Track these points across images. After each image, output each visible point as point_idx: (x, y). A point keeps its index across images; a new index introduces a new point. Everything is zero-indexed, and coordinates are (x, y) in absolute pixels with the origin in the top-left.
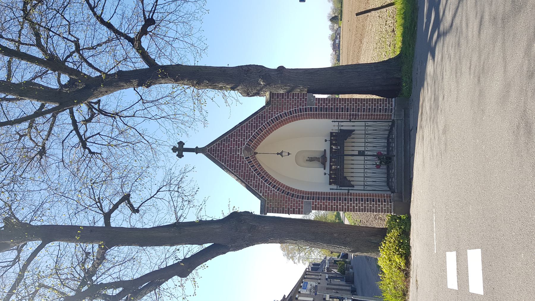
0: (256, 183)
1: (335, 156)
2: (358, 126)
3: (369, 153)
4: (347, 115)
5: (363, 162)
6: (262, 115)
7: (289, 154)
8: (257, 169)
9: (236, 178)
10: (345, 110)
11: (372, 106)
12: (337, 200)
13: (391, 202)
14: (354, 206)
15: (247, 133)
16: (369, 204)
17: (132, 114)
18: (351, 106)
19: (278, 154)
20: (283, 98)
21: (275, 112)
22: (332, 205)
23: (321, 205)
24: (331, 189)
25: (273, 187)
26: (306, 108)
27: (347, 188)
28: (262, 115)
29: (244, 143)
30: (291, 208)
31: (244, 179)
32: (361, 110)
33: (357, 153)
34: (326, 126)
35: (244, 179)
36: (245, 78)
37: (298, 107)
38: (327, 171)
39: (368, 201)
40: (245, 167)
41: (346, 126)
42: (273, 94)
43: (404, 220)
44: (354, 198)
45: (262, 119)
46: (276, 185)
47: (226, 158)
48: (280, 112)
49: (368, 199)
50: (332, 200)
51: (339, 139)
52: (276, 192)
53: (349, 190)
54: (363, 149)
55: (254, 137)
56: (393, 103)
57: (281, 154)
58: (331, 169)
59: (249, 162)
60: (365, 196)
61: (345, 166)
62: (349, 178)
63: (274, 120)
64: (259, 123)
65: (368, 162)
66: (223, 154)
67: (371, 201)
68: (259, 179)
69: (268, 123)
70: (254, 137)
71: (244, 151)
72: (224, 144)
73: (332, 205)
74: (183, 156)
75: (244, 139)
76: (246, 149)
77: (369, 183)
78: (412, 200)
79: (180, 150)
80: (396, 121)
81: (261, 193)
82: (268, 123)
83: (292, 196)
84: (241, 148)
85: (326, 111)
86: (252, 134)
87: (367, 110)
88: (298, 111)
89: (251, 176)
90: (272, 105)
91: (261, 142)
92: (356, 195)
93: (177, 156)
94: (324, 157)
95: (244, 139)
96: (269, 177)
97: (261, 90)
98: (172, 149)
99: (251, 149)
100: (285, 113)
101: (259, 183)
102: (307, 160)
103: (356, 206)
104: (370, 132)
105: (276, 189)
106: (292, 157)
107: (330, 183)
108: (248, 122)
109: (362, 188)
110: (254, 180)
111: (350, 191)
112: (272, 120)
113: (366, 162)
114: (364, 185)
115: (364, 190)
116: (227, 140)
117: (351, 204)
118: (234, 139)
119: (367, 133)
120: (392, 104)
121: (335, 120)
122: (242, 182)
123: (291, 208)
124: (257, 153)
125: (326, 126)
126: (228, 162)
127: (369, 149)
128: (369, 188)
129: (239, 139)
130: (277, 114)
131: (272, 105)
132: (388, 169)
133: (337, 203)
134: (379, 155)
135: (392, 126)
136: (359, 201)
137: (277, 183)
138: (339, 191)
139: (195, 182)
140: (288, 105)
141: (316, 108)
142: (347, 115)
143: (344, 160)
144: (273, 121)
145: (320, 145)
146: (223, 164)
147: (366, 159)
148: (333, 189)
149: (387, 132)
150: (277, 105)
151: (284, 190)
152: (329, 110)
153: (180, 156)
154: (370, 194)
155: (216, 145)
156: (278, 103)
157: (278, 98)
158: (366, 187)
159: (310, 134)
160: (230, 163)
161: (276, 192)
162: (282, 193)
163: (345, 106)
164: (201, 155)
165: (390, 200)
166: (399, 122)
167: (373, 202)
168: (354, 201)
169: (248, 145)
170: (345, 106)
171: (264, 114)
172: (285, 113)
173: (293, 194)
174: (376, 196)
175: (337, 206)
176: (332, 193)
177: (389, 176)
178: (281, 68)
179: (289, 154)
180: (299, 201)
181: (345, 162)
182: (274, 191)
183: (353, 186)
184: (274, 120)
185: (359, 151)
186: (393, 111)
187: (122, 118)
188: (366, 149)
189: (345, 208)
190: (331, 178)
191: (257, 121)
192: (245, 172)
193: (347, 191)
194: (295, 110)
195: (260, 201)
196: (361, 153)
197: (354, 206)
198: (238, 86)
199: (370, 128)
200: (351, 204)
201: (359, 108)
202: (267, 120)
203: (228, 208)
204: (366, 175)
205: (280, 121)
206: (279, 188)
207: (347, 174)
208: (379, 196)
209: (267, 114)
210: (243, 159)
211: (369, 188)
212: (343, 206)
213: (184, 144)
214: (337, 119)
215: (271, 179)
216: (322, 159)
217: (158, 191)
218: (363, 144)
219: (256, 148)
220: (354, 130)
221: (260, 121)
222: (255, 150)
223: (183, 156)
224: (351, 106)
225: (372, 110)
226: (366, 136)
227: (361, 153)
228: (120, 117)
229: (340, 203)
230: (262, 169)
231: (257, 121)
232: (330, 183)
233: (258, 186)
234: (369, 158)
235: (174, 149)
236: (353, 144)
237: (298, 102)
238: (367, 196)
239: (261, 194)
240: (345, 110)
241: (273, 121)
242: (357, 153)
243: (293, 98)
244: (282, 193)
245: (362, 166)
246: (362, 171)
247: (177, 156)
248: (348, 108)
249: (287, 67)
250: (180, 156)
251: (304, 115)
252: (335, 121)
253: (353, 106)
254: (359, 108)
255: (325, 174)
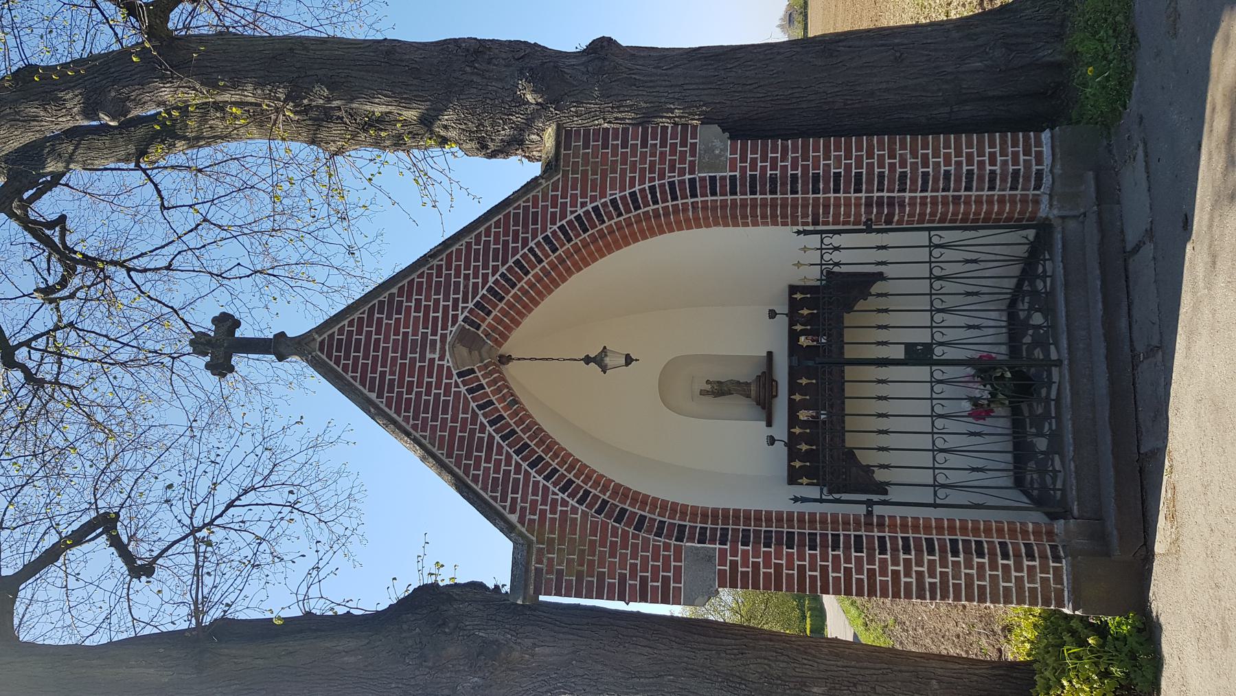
0: (497, 471)
1: (811, 367)
2: (899, 254)
3: (951, 353)
4: (858, 205)
5: (925, 390)
6: (526, 209)
7: (629, 360)
8: (501, 418)
9: (420, 452)
10: (847, 183)
11: (959, 164)
12: (824, 546)
13: (1057, 558)
14: (896, 574)
15: (467, 277)
16: (963, 568)
17: (163, 263)
18: (870, 166)
19: (587, 360)
20: (605, 146)
21: (574, 197)
22: (801, 569)
23: (756, 566)
24: (796, 500)
25: (563, 490)
26: (692, 181)
27: (864, 497)
28: (526, 209)
29: (455, 317)
30: (633, 575)
31: (449, 456)
32: (914, 181)
33: (899, 353)
34: (776, 253)
35: (449, 456)
36: (464, 85)
37: (662, 176)
38: (780, 429)
39: (955, 553)
40: (455, 409)
41: (854, 251)
42: (568, 133)
43: (1124, 639)
44: (757, 533)
45: (525, 226)
46: (573, 478)
47: (383, 374)
48: (593, 199)
49: (954, 543)
50: (801, 545)
51: (823, 310)
52: (574, 510)
53: (870, 503)
54: (923, 337)
55: (495, 294)
56: (1046, 150)
57: (599, 360)
58: (793, 420)
59: (470, 391)
60: (940, 529)
61: (850, 406)
62: (866, 458)
63: (573, 228)
64: (515, 240)
65: (948, 390)
66: (375, 358)
67: (967, 552)
68: (518, 466)
69: (546, 238)
70: (495, 294)
71: (453, 346)
72: (380, 320)
73: (801, 569)
74: (231, 369)
75: (456, 301)
76: (462, 337)
77: (954, 477)
78: (1159, 547)
79: (222, 345)
80: (1056, 223)
81: (512, 511)
82: (546, 238)
83: (639, 527)
84: (444, 337)
85: (773, 192)
86: (485, 281)
87: (936, 180)
88: (663, 192)
89: (483, 450)
90: (565, 174)
91: (523, 316)
92: (904, 527)
93: (208, 366)
94: (766, 380)
95: (456, 301)
96: (549, 449)
97: (529, 124)
98: (192, 343)
99: (484, 340)
100: (613, 201)
101: (507, 473)
102: (703, 393)
103: (908, 575)
104: (950, 269)
105: (572, 496)
106: (646, 373)
107: (793, 479)
108: (471, 238)
109: (926, 496)
110: (488, 460)
111: (878, 510)
112: (562, 228)
113: (938, 388)
114: (936, 486)
115: (935, 506)
116: (393, 306)
117: (883, 563)
118: (418, 301)
119: (937, 272)
120: (1039, 157)
121: (811, 228)
122: (442, 467)
123: (633, 575)
124: (510, 358)
125: (776, 253)
126: (391, 390)
127: (951, 335)
128: (955, 497)
129: (437, 301)
130: (583, 205)
131: (565, 174)
132: (1017, 425)
133: (824, 558)
134: (984, 368)
135: (1037, 250)
136: (919, 551)
137: (580, 472)
138: (828, 508)
139: (352, 478)
140: (623, 171)
141: (733, 178)
142: (858, 205)
143: (843, 382)
144: (565, 233)
145: (755, 337)
146: (373, 396)
147: (938, 375)
148: (804, 500)
149: (1016, 270)
150: (585, 173)
151: (605, 502)
152: (784, 184)
153: (221, 368)
154: (927, 520)
155: (351, 324)
156: (586, 163)
157: (586, 146)
158: (941, 493)
159: (710, 280)
160: (400, 394)
161: (574, 510)
162: (599, 512)
163: (848, 167)
164: (296, 365)
165: (1054, 548)
166: (1072, 224)
167: (980, 554)
168: (895, 549)
169: (472, 323)
170: (848, 167)
171: (535, 205)
172: (613, 201)
173: (643, 518)
174: (988, 531)
175: (824, 570)
176: (801, 516)
177: (1021, 452)
178: (603, 47)
179: (629, 360)
180: (667, 547)
181: (849, 390)
182: (564, 503)
183: (882, 488)
184: (573, 228)
185: (909, 347)
186: (1047, 180)
187: (132, 273)
188: (938, 338)
189: (860, 581)
190: (793, 454)
191: (506, 234)
192: (453, 430)
193: (861, 510)
194: (652, 188)
195: (511, 544)
196: (918, 355)
197: (896, 574)
198: (441, 111)
199: (949, 254)
200: (883, 563)
201: (903, 176)
202: (544, 230)
203: (415, 567)
204: (940, 444)
205: (595, 235)
206: (587, 493)
207: (863, 439)
208: (1000, 531)
209: (545, 208)
210: (450, 376)
211: (955, 497)
212: (848, 571)
213: (237, 324)
214: (815, 223)
215: (556, 455)
216: (759, 391)
217: (231, 505)
218: (925, 319)
219: (505, 338)
220: (880, 276)
221: (516, 233)
222: (500, 345)
223: (231, 369)
224: (870, 166)
225: (958, 180)
226: (937, 284)
227: (918, 355)
228: (129, 270)
229: (836, 558)
230: (524, 418)
231: (506, 234)
232: (793, 479)
233: (503, 485)
234: (951, 372)
235: (200, 344)
236: (883, 319)
237: (662, 161)
238: (952, 530)
239: (514, 518)
240: (847, 183)
241: (565, 233)
242: (899, 353)
243: (644, 145)
244: (599, 512)
245: (924, 270)
246: (913, 424)
247: (208, 366)
248: (859, 175)
249: (625, 39)
250: (221, 368)
251: (685, 210)
252: (806, 233)
253: (881, 165)
254: (903, 176)
255: (772, 441)
